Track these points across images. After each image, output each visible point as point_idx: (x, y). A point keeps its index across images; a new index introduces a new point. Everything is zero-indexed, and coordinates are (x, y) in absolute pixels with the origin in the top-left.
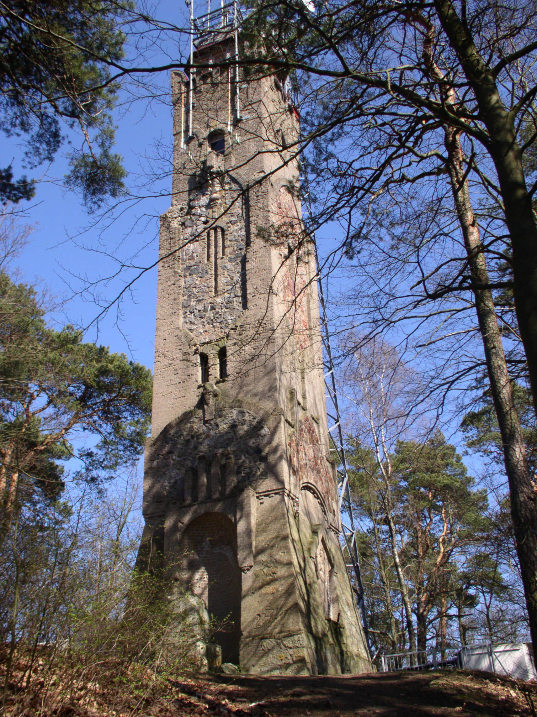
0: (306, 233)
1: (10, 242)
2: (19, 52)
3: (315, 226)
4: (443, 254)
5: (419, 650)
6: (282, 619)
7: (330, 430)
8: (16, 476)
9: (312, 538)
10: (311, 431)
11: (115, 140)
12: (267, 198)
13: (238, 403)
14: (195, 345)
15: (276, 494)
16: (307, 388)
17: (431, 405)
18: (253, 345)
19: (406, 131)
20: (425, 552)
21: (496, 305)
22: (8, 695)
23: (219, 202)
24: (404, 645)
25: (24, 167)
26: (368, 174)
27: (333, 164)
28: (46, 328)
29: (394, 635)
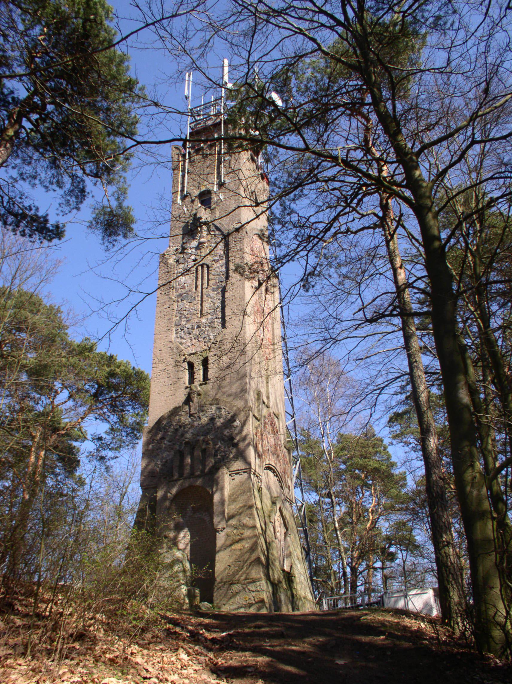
0: (273, 270)
1: (44, 271)
2: (59, 129)
3: (279, 265)
4: (379, 289)
5: (351, 594)
6: (247, 569)
7: (287, 424)
8: (43, 453)
9: (272, 507)
10: (272, 424)
11: (128, 195)
12: (242, 243)
13: (216, 401)
14: (184, 355)
15: (244, 472)
16: (270, 390)
17: (366, 406)
18: (229, 356)
19: (351, 195)
20: (358, 519)
21: (417, 329)
22: (35, 621)
23: (206, 245)
24: (340, 590)
25: (58, 215)
26: (321, 226)
27: (294, 218)
28: (69, 339)
29: (332, 583)
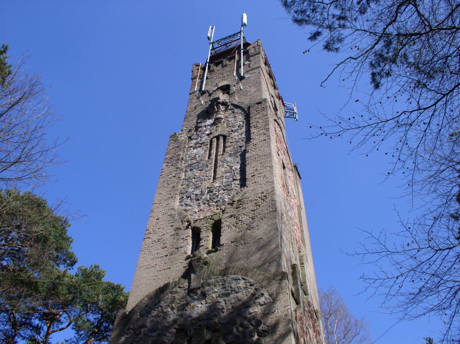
28: (70, 250)
